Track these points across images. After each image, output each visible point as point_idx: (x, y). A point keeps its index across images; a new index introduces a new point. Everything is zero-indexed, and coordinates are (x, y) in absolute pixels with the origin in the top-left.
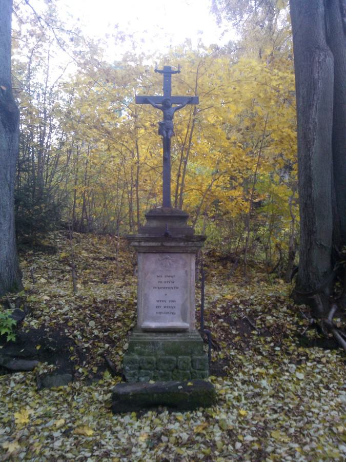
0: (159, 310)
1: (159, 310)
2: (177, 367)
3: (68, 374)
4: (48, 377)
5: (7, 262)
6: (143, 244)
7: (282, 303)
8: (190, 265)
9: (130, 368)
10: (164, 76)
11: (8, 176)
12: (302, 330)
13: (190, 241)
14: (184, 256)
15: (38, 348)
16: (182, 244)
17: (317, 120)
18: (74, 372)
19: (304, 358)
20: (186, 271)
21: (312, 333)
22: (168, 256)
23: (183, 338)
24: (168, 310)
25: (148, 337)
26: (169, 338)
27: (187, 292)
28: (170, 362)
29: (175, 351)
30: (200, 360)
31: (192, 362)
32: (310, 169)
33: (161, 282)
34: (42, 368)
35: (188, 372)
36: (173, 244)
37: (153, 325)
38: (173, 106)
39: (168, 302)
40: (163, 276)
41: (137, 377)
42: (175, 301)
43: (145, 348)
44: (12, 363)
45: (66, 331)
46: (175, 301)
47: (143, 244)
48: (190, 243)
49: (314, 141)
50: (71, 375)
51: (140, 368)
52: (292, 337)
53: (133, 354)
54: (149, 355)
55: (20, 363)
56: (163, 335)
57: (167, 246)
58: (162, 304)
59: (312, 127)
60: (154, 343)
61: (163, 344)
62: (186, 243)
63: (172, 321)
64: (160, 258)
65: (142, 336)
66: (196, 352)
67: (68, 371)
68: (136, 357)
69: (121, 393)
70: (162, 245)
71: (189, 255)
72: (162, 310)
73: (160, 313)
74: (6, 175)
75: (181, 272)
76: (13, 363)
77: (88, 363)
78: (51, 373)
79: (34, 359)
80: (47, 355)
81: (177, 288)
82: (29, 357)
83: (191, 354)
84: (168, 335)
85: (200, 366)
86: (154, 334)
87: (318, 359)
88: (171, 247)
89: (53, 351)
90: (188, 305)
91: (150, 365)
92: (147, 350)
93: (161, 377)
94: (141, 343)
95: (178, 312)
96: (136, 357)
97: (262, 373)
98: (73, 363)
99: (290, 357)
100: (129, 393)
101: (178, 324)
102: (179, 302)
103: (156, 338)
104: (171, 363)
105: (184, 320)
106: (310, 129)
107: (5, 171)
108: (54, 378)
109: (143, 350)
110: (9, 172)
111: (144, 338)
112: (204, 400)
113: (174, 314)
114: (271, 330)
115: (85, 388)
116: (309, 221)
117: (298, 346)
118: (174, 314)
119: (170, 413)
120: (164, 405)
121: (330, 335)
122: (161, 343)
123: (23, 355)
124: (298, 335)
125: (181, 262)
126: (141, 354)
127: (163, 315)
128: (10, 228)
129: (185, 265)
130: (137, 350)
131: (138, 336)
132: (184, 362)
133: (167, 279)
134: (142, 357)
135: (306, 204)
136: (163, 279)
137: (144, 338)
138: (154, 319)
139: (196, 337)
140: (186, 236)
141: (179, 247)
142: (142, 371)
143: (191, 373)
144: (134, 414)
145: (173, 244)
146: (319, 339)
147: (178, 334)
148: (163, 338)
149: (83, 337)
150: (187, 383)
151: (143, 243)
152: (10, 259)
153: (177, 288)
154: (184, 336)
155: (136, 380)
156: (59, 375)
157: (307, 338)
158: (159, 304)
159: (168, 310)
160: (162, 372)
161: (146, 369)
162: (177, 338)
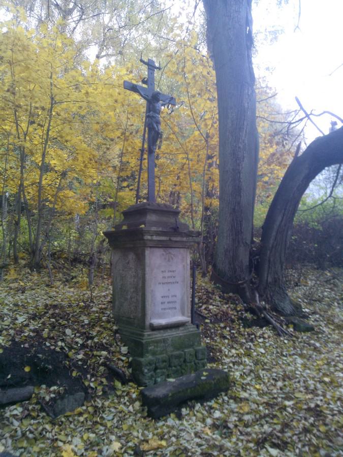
0: (163, 306)
1: (163, 306)
2: (185, 361)
3: (80, 393)
4: (59, 402)
6: (155, 238)
7: (213, 294)
8: (187, 260)
9: (148, 370)
12: (242, 314)
13: (190, 236)
14: (182, 250)
15: (27, 369)
16: (185, 239)
17: (246, 142)
18: (86, 389)
20: (184, 266)
21: (248, 315)
23: (185, 331)
24: (171, 305)
25: (158, 335)
26: (174, 333)
28: (178, 357)
29: (181, 345)
32: (240, 181)
33: (165, 278)
34: (46, 393)
36: (178, 239)
37: (163, 322)
38: (161, 102)
40: (167, 271)
41: (154, 379)
42: (176, 296)
43: (157, 347)
45: (48, 344)
46: (176, 296)
47: (155, 238)
48: (191, 238)
49: (244, 158)
50: (83, 394)
51: (156, 368)
53: (147, 355)
54: (161, 353)
55: (12, 393)
56: (169, 331)
58: (166, 300)
59: (242, 147)
60: (164, 341)
63: (174, 316)
64: (164, 253)
65: (152, 335)
67: (78, 390)
69: (161, 396)
71: (186, 250)
72: (166, 306)
73: (165, 309)
75: (180, 267)
77: (92, 376)
78: (60, 396)
79: (26, 385)
80: (42, 376)
81: (178, 282)
82: (19, 383)
84: (174, 330)
86: (162, 331)
88: (176, 242)
89: (50, 370)
90: (186, 299)
91: (165, 363)
93: (174, 374)
94: (153, 342)
95: (178, 306)
98: (78, 380)
100: (168, 395)
103: (165, 335)
104: (180, 358)
105: (183, 314)
106: (239, 147)
108: (66, 400)
109: (156, 349)
111: (154, 336)
112: (219, 387)
113: (175, 308)
114: (219, 317)
115: (107, 403)
116: (237, 223)
119: (202, 405)
120: (191, 399)
121: (263, 315)
122: (170, 339)
123: (11, 382)
125: (180, 257)
126: (154, 354)
127: (167, 311)
130: (151, 350)
131: (149, 335)
132: (191, 355)
133: (170, 274)
134: (158, 356)
135: (234, 209)
136: (167, 274)
137: (154, 336)
138: (161, 316)
142: (158, 371)
143: (195, 364)
145: (178, 239)
147: (181, 328)
148: (169, 334)
151: (154, 237)
154: (185, 330)
155: (153, 382)
156: (70, 396)
157: (248, 320)
159: (171, 305)
160: (173, 368)
161: (161, 369)
162: (180, 332)
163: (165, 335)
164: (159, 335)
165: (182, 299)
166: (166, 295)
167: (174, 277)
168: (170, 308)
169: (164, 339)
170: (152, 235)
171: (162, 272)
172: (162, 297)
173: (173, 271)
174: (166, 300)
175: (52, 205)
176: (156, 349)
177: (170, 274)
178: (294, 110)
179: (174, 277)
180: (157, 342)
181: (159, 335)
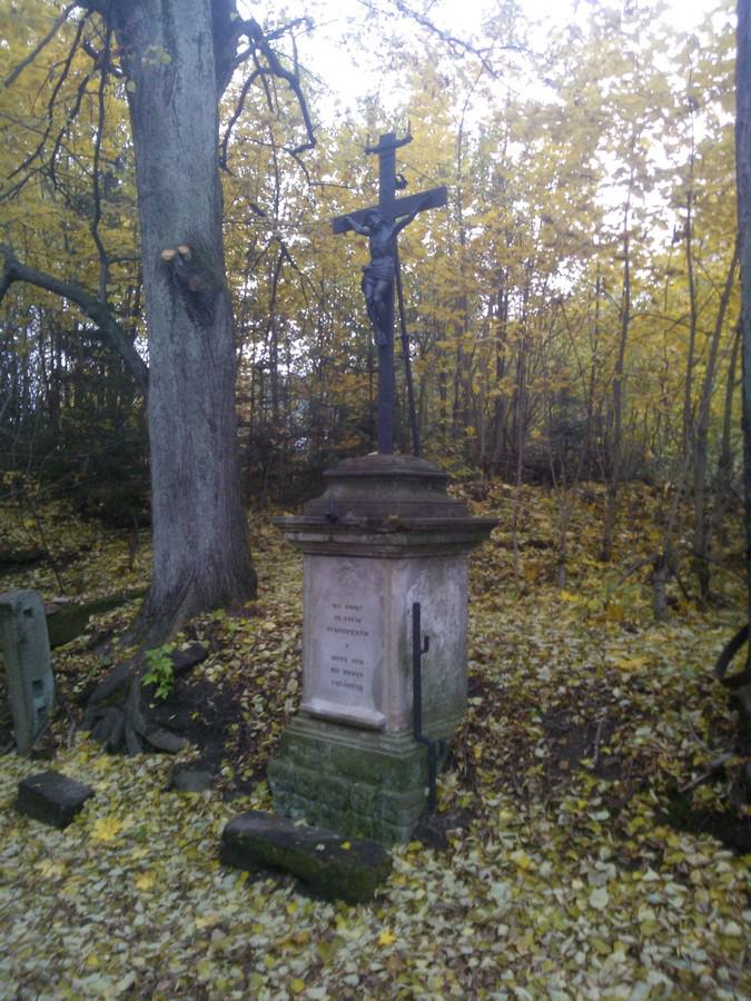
0: (335, 677)
1: (335, 677)
5: (211, 556)
6: (302, 537)
10: (381, 158)
11: (207, 405)
13: (376, 533)
14: (378, 564)
16: (364, 539)
19: (651, 855)
20: (382, 599)
22: (347, 563)
23: (369, 744)
24: (351, 679)
25: (314, 732)
27: (383, 646)
28: (336, 788)
30: (389, 799)
31: (375, 799)
35: (369, 819)
39: (349, 661)
42: (361, 662)
44: (155, 735)
46: (361, 662)
48: (378, 536)
52: (657, 793)
54: (311, 766)
56: (337, 730)
57: (342, 543)
58: (341, 665)
60: (318, 745)
61: (333, 751)
62: (371, 537)
66: (388, 781)
68: (291, 766)
70: (331, 539)
71: (388, 562)
72: (340, 677)
73: (338, 684)
74: (200, 404)
76: (158, 738)
81: (366, 634)
83: (378, 782)
84: (346, 732)
85: (389, 813)
86: (323, 726)
87: (685, 869)
92: (307, 756)
94: (298, 738)
95: (368, 687)
96: (291, 766)
97: (519, 866)
99: (619, 843)
101: (365, 712)
102: (368, 667)
103: (325, 734)
105: (378, 707)
107: (197, 397)
110: (207, 398)
117: (659, 820)
118: (361, 689)
122: (330, 747)
124: (672, 792)
125: (373, 578)
126: (298, 761)
127: (342, 689)
128: (216, 497)
129: (380, 584)
131: (298, 724)
133: (349, 613)
136: (344, 613)
138: (329, 695)
139: (393, 748)
140: (369, 522)
141: (360, 544)
144: (246, 875)
146: (717, 813)
147: (364, 735)
149: (266, 708)
150: (352, 846)
152: (220, 553)
153: (366, 634)
158: (336, 664)
159: (351, 679)
163: (325, 734)
164: (315, 732)
165: (377, 673)
166: (340, 655)
167: (359, 621)
168: (349, 686)
169: (317, 741)
170: (296, 532)
171: (335, 606)
172: (334, 658)
173: (356, 608)
174: (341, 665)
175: (673, 635)
176: (302, 754)
177: (349, 613)
178: (680, 31)
179: (359, 621)
180: (306, 742)
181: (315, 732)
